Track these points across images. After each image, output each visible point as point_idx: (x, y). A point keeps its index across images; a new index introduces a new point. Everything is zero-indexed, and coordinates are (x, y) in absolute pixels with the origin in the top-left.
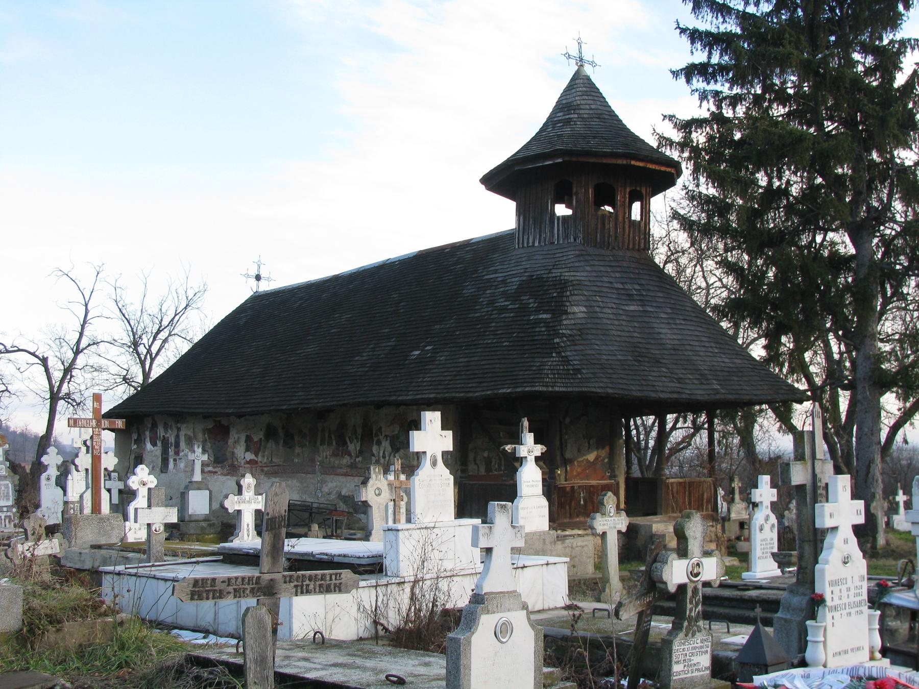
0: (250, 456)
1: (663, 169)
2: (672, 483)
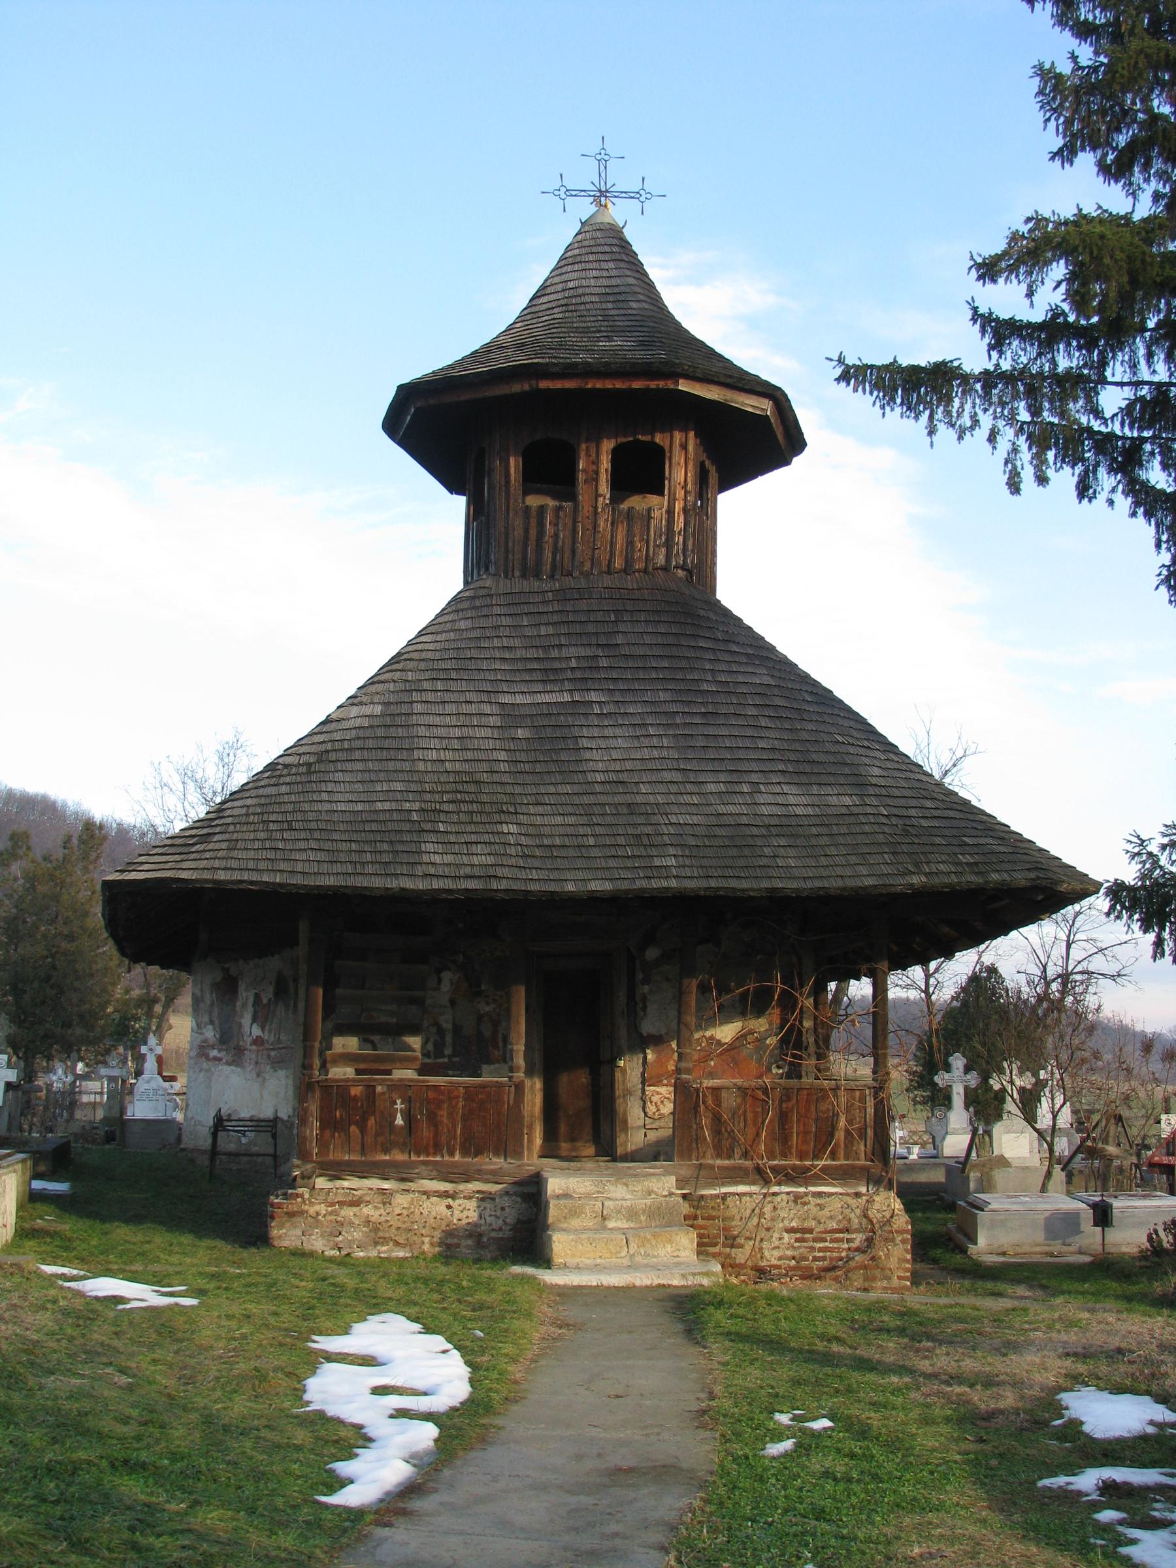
0: (256, 1031)
1: (637, 385)
2: (716, 1090)
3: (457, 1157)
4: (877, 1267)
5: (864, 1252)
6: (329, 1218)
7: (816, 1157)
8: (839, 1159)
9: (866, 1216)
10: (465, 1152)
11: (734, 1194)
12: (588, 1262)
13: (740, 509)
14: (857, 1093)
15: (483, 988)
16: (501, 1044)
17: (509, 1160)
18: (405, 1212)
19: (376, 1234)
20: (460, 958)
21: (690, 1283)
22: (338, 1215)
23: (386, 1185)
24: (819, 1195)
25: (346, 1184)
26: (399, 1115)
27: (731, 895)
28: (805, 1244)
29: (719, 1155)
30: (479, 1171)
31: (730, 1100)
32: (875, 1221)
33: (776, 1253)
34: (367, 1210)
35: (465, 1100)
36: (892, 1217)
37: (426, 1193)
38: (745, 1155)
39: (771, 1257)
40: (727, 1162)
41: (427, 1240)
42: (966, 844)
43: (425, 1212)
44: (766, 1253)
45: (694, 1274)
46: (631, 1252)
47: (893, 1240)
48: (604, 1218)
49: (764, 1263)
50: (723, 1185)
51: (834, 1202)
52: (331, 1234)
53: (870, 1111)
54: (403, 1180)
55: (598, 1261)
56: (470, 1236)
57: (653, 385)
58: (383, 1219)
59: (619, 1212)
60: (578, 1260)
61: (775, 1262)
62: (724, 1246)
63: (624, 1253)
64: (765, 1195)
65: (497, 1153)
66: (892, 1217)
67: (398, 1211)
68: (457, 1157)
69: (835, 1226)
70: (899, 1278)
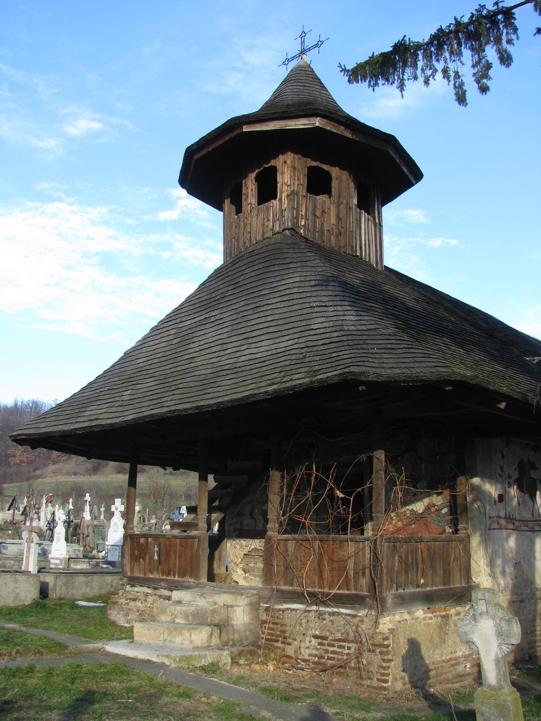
1: (227, 138)
3: (176, 578)
6: (126, 606)
12: (146, 641)
13: (395, 213)
29: (285, 584)
33: (308, 651)
34: (138, 603)
40: (291, 588)
44: (302, 650)
47: (374, 651)
50: (286, 602)
54: (155, 589)
57: (233, 135)
58: (144, 609)
60: (142, 639)
61: (307, 657)
65: (191, 577)
67: (149, 605)
68: (176, 578)
70: (378, 679)
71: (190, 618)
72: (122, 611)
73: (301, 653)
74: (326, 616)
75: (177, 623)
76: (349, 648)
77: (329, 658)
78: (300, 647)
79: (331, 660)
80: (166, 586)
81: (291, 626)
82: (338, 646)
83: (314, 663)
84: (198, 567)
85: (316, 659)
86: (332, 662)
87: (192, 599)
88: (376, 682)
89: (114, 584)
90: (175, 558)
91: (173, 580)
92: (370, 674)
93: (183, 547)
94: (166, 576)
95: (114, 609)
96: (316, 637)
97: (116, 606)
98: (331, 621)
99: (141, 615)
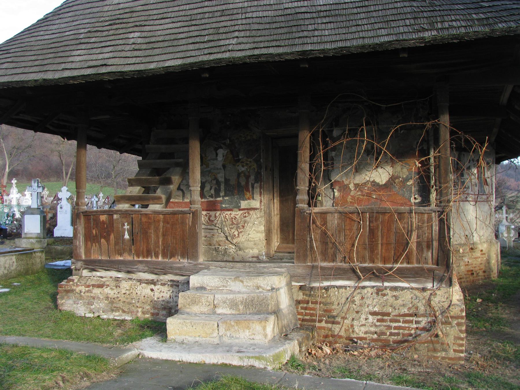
3: (160, 259)
4: (438, 342)
5: (428, 330)
6: (87, 294)
7: (396, 261)
8: (412, 263)
9: (430, 305)
10: (164, 256)
11: (334, 287)
12: (190, 339)
14: (426, 216)
15: (240, 157)
16: (251, 189)
17: (189, 261)
18: (128, 292)
19: (113, 304)
20: (228, 141)
21: (245, 364)
22: (92, 292)
23: (120, 275)
24: (395, 289)
25: (98, 274)
26: (126, 232)
27: (271, 60)
28: (385, 324)
29: (325, 260)
30: (171, 268)
31: (334, 221)
32: (436, 309)
33: (363, 329)
34: (107, 290)
35: (164, 222)
36: (449, 306)
37: (140, 281)
38: (344, 260)
39: (360, 331)
41: (140, 310)
42: (482, 7)
43: (139, 293)
44: (356, 329)
45: (249, 358)
46: (220, 334)
48: (215, 306)
49: (353, 336)
50: (327, 280)
51: (405, 295)
52: (88, 304)
53: (436, 228)
54: (129, 272)
55: (197, 339)
56: (165, 309)
58: (116, 296)
59: (224, 302)
62: (327, 322)
63: (215, 334)
64: (356, 288)
65: (183, 257)
66: (449, 306)
67: (124, 291)
68: (160, 259)
69: (407, 312)
71: (241, 307)
72: (81, 299)
73: (353, 331)
74: (388, 291)
75: (219, 314)
76: (417, 322)
77: (391, 334)
78: (352, 326)
79: (394, 336)
80: (146, 268)
81: (339, 304)
82: (403, 321)
83: (373, 340)
84: (195, 245)
85: (375, 336)
86: (396, 337)
87: (221, 284)
88: (453, 353)
89: (7, 266)
90: (157, 237)
91: (156, 261)
92: (445, 346)
93: (168, 223)
94: (144, 257)
95: (69, 298)
96: (374, 314)
97: (70, 294)
98: (394, 296)
99: (112, 303)
